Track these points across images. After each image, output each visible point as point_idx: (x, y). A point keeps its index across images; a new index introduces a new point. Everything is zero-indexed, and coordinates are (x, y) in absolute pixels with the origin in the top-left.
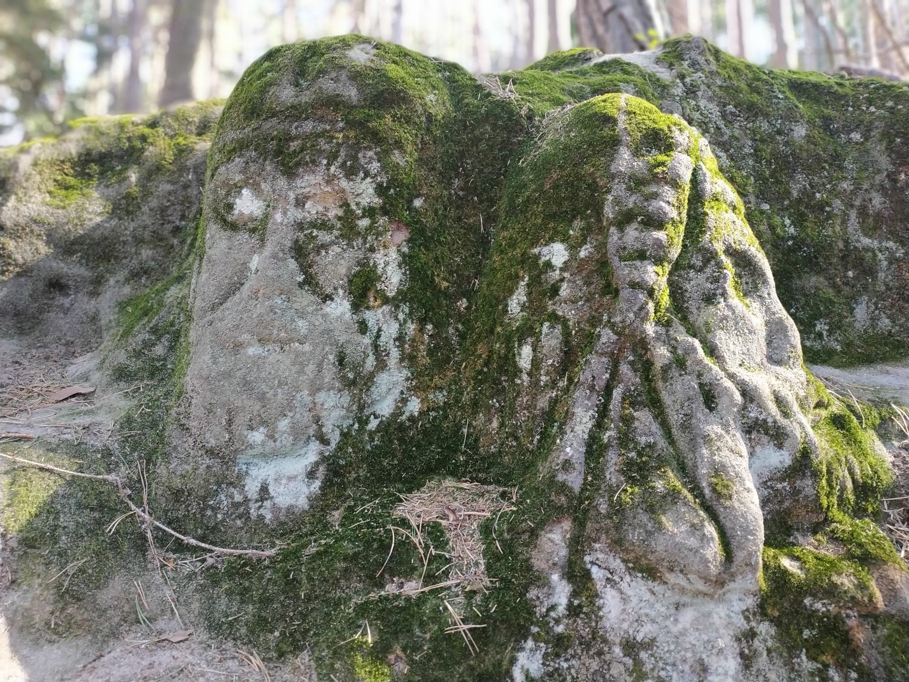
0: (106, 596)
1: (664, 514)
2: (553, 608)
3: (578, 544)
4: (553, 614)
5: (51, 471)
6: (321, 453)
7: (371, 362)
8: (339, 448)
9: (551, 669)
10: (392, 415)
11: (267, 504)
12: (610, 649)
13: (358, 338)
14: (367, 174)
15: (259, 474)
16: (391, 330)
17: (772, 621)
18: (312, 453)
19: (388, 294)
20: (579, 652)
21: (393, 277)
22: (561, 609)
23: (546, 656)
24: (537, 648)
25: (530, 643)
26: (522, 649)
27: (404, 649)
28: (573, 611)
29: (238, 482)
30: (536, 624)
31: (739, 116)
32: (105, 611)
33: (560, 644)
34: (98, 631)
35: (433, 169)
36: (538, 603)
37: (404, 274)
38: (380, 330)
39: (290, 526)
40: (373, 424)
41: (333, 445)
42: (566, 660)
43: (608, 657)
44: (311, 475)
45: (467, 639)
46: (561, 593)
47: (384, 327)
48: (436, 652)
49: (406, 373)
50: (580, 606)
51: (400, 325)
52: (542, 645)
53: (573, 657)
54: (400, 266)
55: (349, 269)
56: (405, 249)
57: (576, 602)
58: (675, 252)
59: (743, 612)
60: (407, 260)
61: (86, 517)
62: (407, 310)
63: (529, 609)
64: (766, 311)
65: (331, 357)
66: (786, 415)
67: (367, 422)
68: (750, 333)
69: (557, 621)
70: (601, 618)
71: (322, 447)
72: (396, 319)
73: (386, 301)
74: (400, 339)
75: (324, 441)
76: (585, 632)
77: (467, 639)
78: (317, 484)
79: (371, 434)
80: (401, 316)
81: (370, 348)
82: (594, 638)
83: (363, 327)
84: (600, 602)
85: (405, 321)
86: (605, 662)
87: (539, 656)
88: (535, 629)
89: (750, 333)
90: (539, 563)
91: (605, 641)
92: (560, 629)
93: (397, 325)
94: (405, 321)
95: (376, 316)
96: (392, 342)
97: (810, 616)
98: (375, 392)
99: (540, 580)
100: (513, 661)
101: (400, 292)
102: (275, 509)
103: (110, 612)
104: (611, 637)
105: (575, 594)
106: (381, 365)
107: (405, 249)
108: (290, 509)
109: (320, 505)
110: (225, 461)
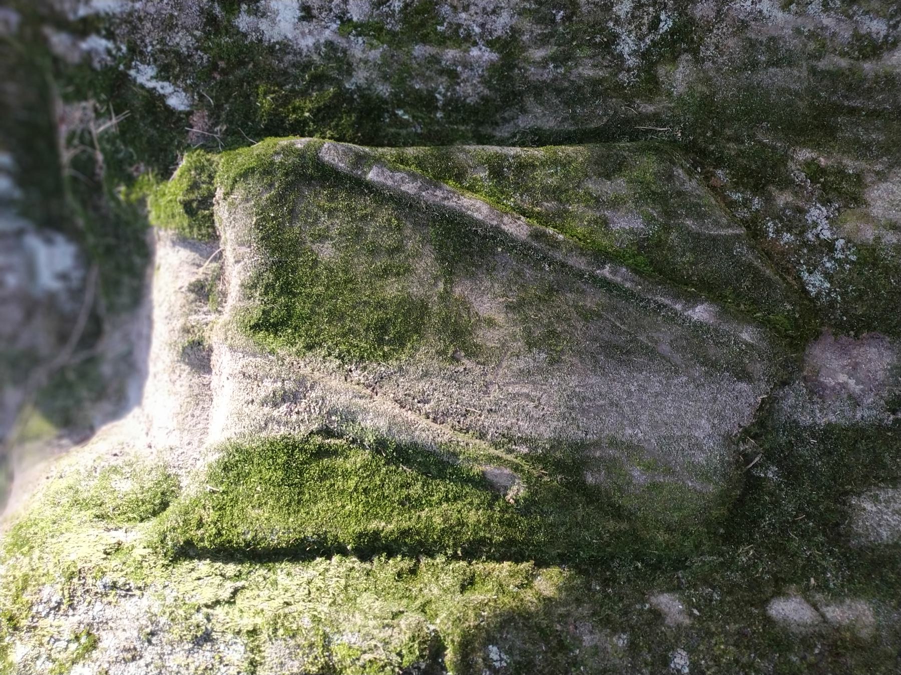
1: (493, 64)
2: (109, 52)
3: (61, 24)
4: (114, 52)
9: (151, 59)
12: (136, 11)
15: (47, 280)
18: (34, 242)
20: (139, 36)
22: (110, 45)
23: (143, 62)
24: (136, 67)
25: (132, 72)
26: (135, 79)
27: (131, 165)
28: (110, 36)
29: (52, 297)
30: (118, 65)
33: (135, 51)
36: (103, 63)
39: (85, 258)
42: (146, 46)
43: (142, 14)
44: (49, 242)
45: (121, 117)
46: (97, 43)
48: (132, 142)
50: (107, 30)
52: (133, 63)
53: (143, 41)
57: (104, 32)
63: (107, 69)
69: (119, 49)
70: (114, 14)
76: (124, 29)
77: (121, 117)
82: (130, 22)
84: (102, 14)
86: (145, 17)
87: (141, 67)
88: (122, 67)
90: (74, 58)
91: (130, 14)
92: (124, 48)
99: (88, 56)
100: (142, 86)
104: (128, 9)
105: (98, 32)
109: (75, 236)
110: (33, 305)
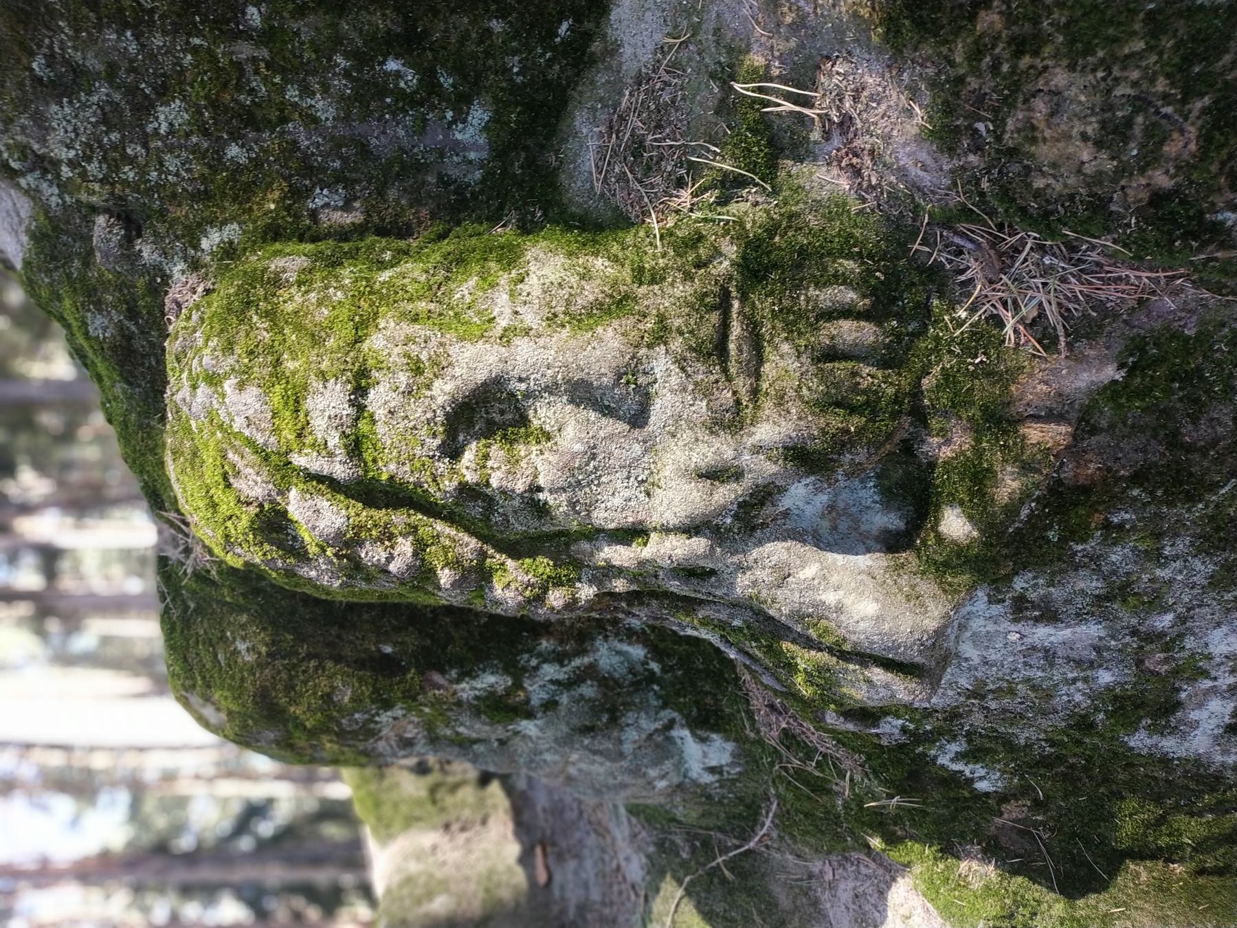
0: (785, 902)
5: (677, 905)
6: (682, 726)
7: (588, 690)
8: (680, 711)
10: (645, 646)
11: (726, 769)
13: (562, 710)
14: (371, 721)
16: (550, 671)
17: (1017, 573)
19: (510, 683)
21: (490, 680)
31: (51, 47)
32: (796, 907)
34: (810, 915)
35: (339, 637)
37: (484, 671)
38: (552, 682)
40: (655, 666)
41: (675, 715)
44: (703, 740)
47: (548, 678)
49: (599, 642)
51: (544, 662)
54: (474, 678)
55: (484, 723)
56: (454, 673)
58: (469, 545)
59: (990, 602)
60: (468, 673)
61: (718, 893)
62: (526, 656)
64: (551, 393)
65: (586, 742)
66: (738, 475)
67: (652, 673)
68: (594, 457)
71: (677, 726)
72: (536, 668)
73: (518, 685)
74: (560, 658)
75: (670, 725)
78: (714, 736)
79: (664, 670)
80: (534, 662)
81: (573, 693)
83: (550, 705)
85: (540, 655)
89: (594, 457)
93: (545, 666)
94: (540, 655)
95: (536, 691)
96: (565, 669)
97: (1034, 527)
98: (621, 672)
101: (506, 671)
102: (732, 765)
103: (798, 903)
106: (590, 672)
107: (454, 673)
108: (733, 755)
